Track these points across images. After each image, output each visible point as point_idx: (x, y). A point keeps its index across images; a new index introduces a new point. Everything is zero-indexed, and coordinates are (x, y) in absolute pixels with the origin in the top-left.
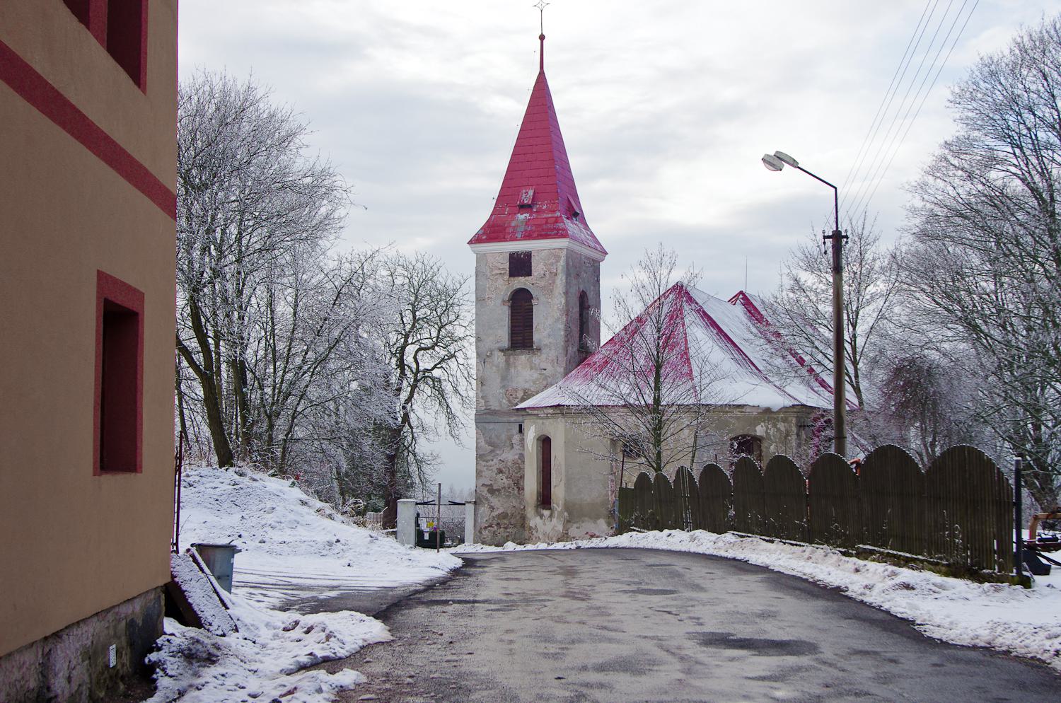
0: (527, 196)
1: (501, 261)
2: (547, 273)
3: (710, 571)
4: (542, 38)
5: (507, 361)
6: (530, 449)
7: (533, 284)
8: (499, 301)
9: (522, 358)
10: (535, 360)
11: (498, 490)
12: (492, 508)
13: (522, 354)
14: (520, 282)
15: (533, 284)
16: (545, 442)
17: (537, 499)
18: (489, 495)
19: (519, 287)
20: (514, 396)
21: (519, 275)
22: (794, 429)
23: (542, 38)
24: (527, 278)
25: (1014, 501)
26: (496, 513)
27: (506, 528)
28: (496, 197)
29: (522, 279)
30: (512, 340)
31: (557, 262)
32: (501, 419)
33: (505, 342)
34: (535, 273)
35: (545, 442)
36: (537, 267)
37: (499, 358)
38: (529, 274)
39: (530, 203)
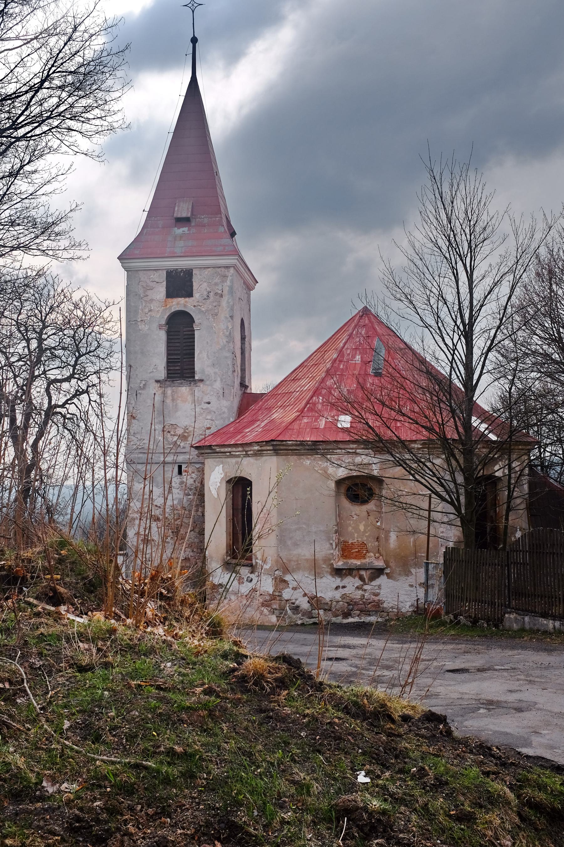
0: (183, 210)
1: (157, 280)
3: (458, 665)
4: (194, 40)
5: (164, 393)
6: (214, 493)
7: (195, 306)
8: (155, 325)
9: (184, 390)
10: (198, 390)
13: (181, 385)
15: (195, 306)
16: (240, 487)
17: (227, 552)
19: (177, 309)
20: (172, 433)
21: (178, 296)
23: (194, 40)
24: (187, 299)
28: (147, 209)
29: (182, 300)
30: (168, 370)
31: (223, 282)
32: (294, 443)
33: (162, 374)
34: (196, 295)
35: (240, 487)
36: (199, 285)
37: (153, 388)
39: (189, 215)
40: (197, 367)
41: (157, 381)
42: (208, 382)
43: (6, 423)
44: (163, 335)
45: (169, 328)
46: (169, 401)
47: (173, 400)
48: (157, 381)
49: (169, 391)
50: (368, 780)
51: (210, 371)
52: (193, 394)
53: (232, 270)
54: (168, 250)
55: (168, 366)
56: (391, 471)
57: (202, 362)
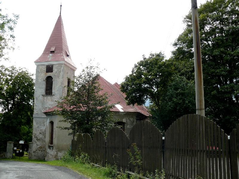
0: (53, 49)
2: (58, 72)
4: (61, 6)
8: (42, 80)
9: (49, 97)
11: (39, 139)
12: (37, 145)
14: (49, 74)
18: (36, 141)
21: (49, 72)
22: (135, 120)
23: (61, 6)
25: (211, 150)
26: (38, 147)
27: (42, 151)
34: (54, 72)
36: (55, 70)
38: (52, 72)
40: (53, 91)
41: (42, 95)
42: (55, 96)
43: (131, 109)
44: (45, 83)
45: (47, 81)
46: (45, 101)
47: (46, 100)
48: (42, 95)
49: (45, 98)
50: (223, 108)
51: (56, 93)
52: (51, 99)
53: (63, 66)
54: (47, 60)
55: (46, 91)
56: (145, 123)
57: (54, 91)
